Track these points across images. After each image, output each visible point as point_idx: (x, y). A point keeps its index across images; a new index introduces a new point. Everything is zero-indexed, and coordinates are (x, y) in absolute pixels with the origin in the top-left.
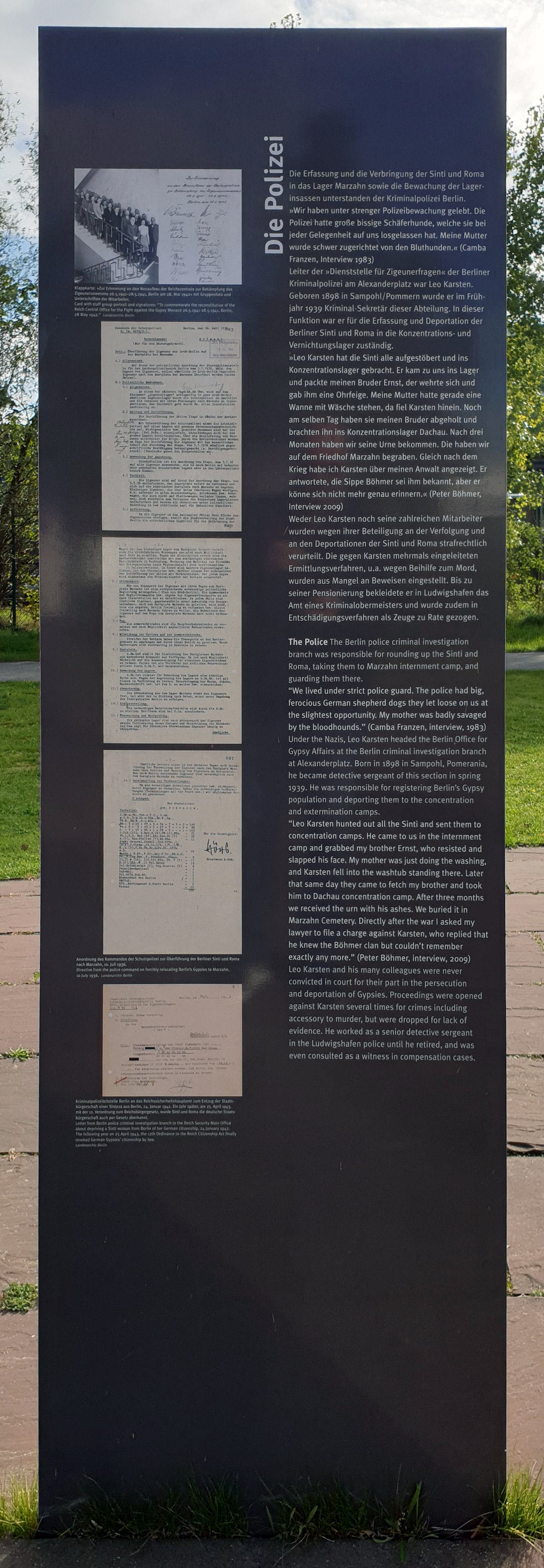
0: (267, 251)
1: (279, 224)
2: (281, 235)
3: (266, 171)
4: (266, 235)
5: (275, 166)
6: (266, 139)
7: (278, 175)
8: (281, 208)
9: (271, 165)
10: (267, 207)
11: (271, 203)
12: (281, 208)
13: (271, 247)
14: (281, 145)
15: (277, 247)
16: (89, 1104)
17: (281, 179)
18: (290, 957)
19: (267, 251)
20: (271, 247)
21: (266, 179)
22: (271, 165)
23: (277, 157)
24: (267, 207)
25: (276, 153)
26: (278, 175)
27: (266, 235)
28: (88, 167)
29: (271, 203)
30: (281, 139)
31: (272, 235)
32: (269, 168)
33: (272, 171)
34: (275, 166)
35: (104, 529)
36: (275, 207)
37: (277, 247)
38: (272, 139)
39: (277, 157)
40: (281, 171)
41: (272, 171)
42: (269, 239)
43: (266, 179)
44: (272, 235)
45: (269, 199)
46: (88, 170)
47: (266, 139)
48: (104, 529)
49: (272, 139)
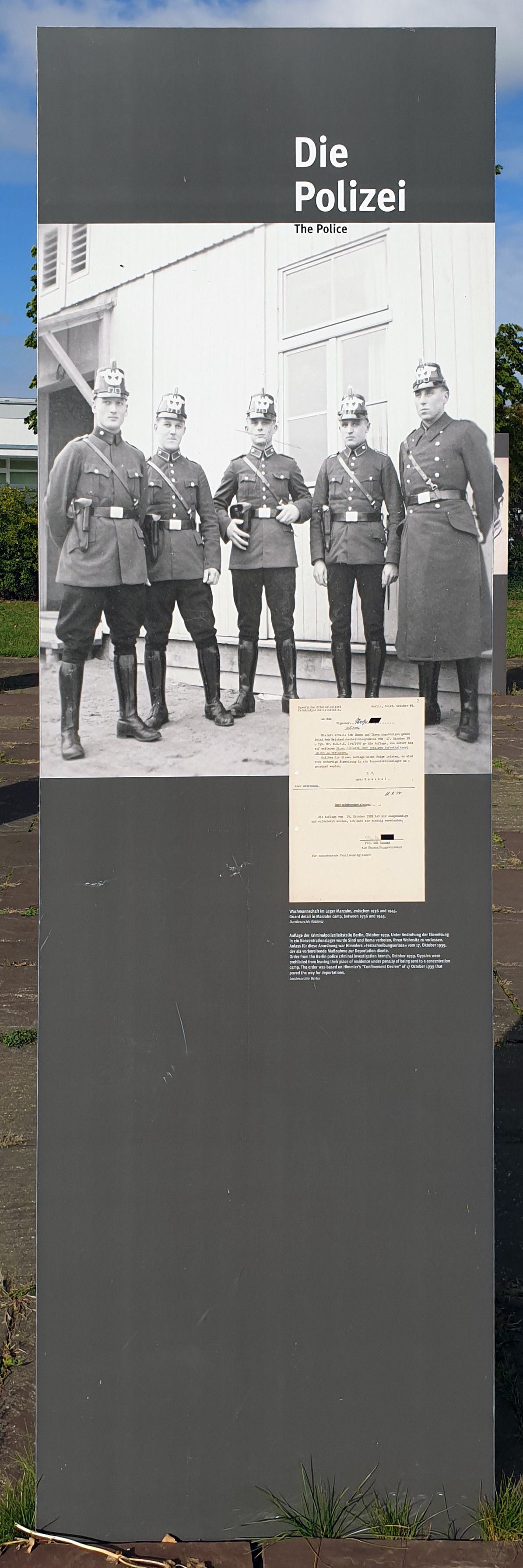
0: (299, 141)
1: (339, 160)
2: (323, 164)
3: (353, 183)
4: (323, 139)
5: (360, 198)
6: (402, 183)
7: (347, 204)
8: (299, 208)
9: (363, 191)
10: (299, 185)
11: (305, 191)
12: (299, 208)
13: (305, 147)
14: (392, 208)
15: (305, 158)
16: (324, 938)
17: (342, 208)
18: (395, 912)
19: (299, 141)
20: (305, 147)
21: (341, 184)
22: (363, 191)
23: (374, 202)
24: (299, 185)
25: (381, 200)
26: (347, 204)
27: (323, 139)
28: (192, 636)
29: (305, 191)
30: (402, 208)
31: (323, 148)
32: (358, 188)
33: (353, 193)
34: (360, 198)
35: (292, 900)
36: (300, 198)
37: (305, 158)
38: (402, 193)
39: (374, 202)
40: (353, 208)
41: (353, 193)
42: (318, 145)
43: (341, 184)
44: (323, 148)
45: (311, 187)
46: (191, 639)
47: (402, 183)
48: (292, 900)
49: (402, 193)
